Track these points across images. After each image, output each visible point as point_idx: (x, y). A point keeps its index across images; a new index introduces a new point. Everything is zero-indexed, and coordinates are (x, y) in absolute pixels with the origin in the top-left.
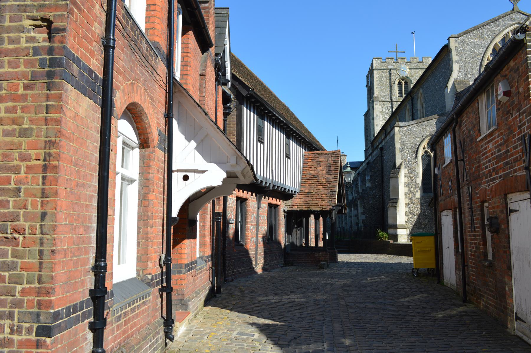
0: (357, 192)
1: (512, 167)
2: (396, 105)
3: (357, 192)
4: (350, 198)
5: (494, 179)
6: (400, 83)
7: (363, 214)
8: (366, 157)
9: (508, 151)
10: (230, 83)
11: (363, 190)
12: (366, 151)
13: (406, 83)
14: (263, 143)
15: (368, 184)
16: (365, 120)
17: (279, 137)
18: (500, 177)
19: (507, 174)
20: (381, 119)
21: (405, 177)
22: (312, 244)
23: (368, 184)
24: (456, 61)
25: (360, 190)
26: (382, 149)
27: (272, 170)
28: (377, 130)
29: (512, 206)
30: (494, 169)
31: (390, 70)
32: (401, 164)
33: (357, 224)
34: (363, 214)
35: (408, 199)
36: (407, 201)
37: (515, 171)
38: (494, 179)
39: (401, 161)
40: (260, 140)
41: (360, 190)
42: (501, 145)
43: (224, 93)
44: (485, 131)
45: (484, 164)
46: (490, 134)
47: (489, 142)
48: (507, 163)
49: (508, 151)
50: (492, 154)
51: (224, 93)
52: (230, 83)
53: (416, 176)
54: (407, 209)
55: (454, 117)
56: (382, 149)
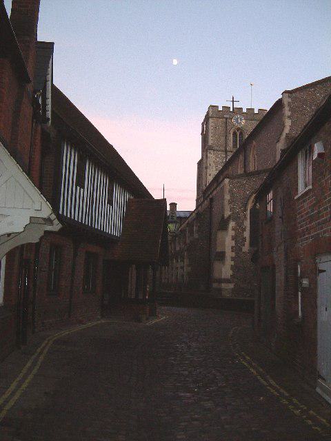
0: (185, 243)
1: (322, 228)
2: (230, 155)
3: (185, 243)
4: (178, 249)
5: (307, 239)
6: (235, 134)
7: (188, 266)
8: (197, 206)
9: (319, 212)
10: (50, 122)
11: (191, 241)
12: (197, 200)
13: (241, 134)
14: (84, 188)
15: (196, 236)
16: (198, 168)
17: (101, 180)
18: (312, 237)
19: (318, 234)
20: (214, 169)
21: (233, 229)
22: (87, 224)
23: (196, 236)
24: (289, 117)
25: (188, 241)
26: (212, 200)
27: (82, 211)
28: (210, 179)
29: (321, 267)
30: (307, 229)
31: (226, 119)
32: (230, 216)
33: (183, 276)
34: (188, 266)
35: (234, 253)
36: (234, 255)
37: (325, 232)
38: (307, 239)
39: (230, 213)
40: (80, 182)
41: (188, 241)
42: (315, 205)
43: (43, 131)
44: (301, 190)
45: (299, 223)
46: (306, 194)
47: (304, 201)
48: (319, 224)
49: (319, 212)
50: (307, 214)
51: (43, 131)
52: (50, 122)
53: (244, 230)
54: (233, 263)
55: (207, 256)
56: (212, 200)
